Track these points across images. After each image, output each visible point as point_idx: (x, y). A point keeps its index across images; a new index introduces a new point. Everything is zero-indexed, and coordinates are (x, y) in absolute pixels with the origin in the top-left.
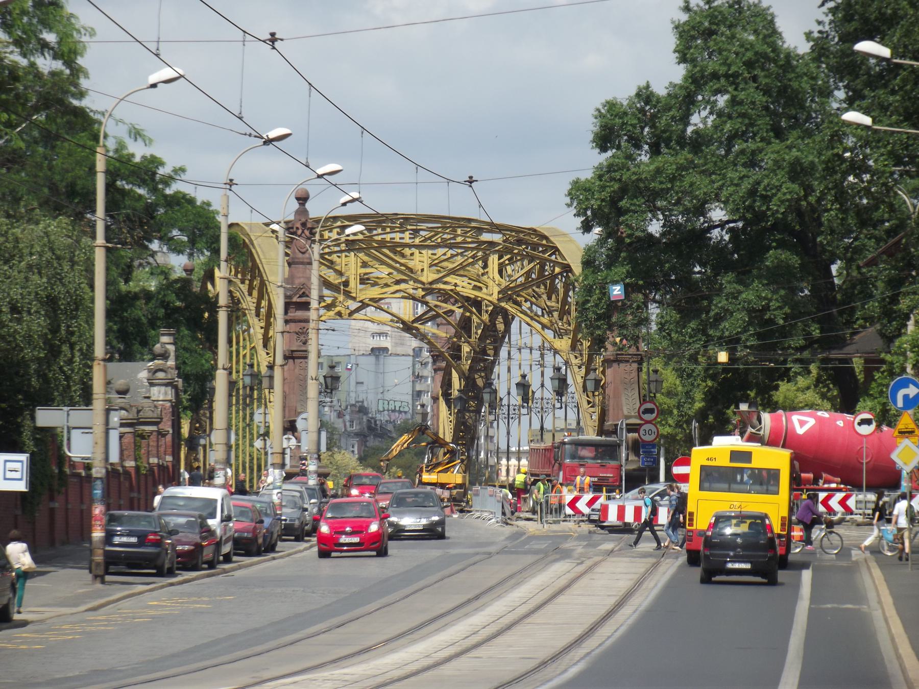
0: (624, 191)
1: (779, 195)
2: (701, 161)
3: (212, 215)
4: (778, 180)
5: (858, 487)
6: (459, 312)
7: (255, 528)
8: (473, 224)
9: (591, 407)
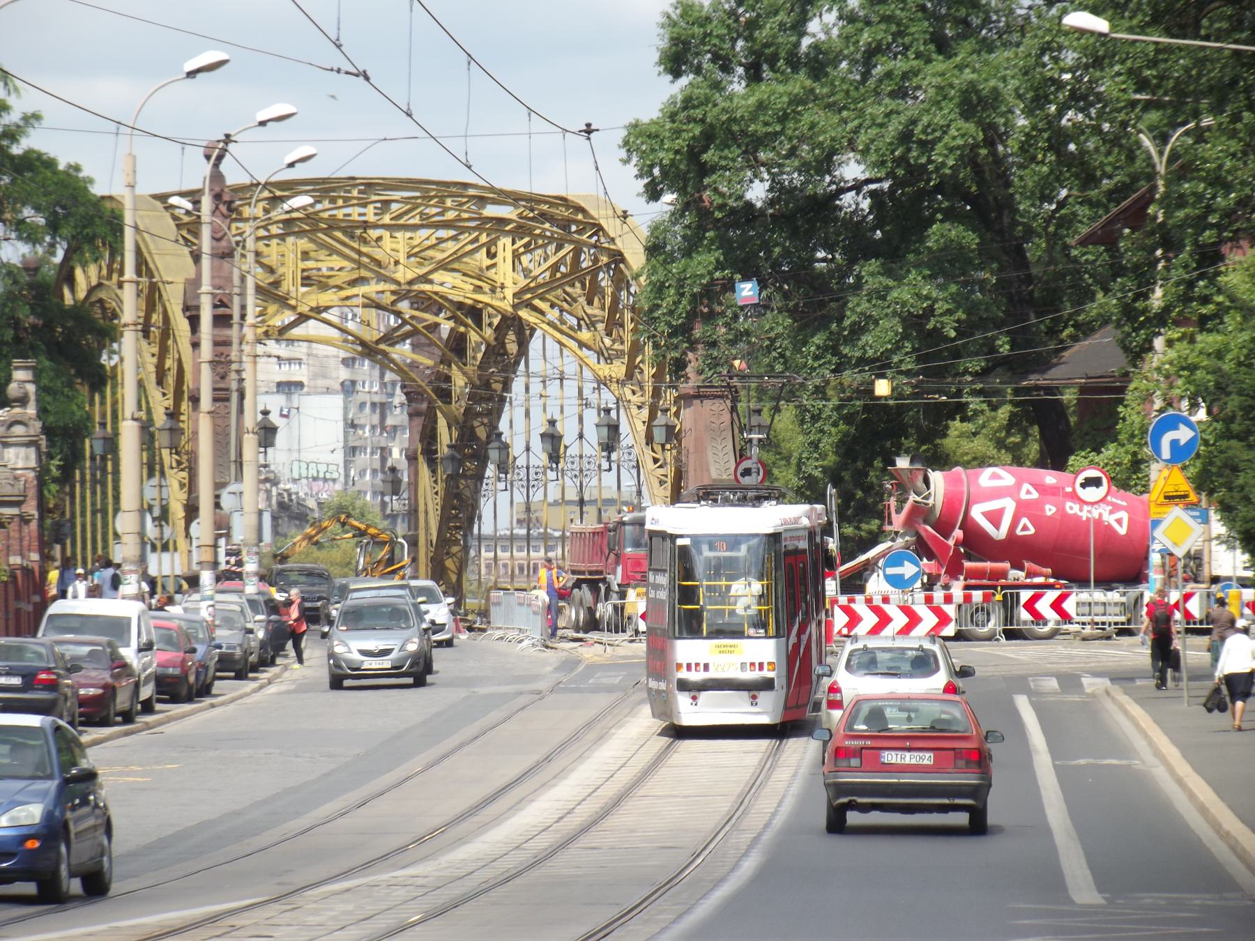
0: (708, 137)
1: (946, 139)
2: (825, 90)
3: (82, 184)
5: (1083, 582)
6: (446, 327)
7: (184, 661)
8: (472, 192)
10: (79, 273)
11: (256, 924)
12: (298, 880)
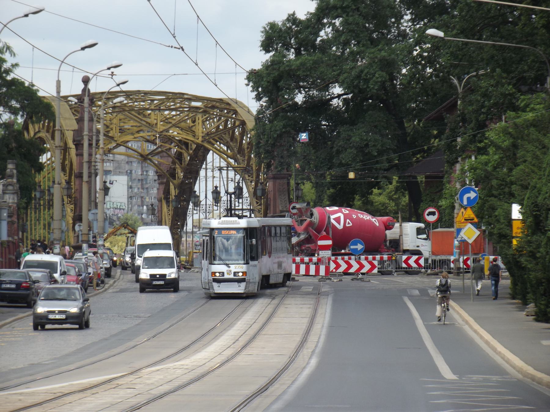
1: (374, 78)
4: (374, 70)
6: (174, 150)
8: (186, 96)
9: (259, 205)
10: (31, 126)
11: (127, 383)
12: (137, 365)
